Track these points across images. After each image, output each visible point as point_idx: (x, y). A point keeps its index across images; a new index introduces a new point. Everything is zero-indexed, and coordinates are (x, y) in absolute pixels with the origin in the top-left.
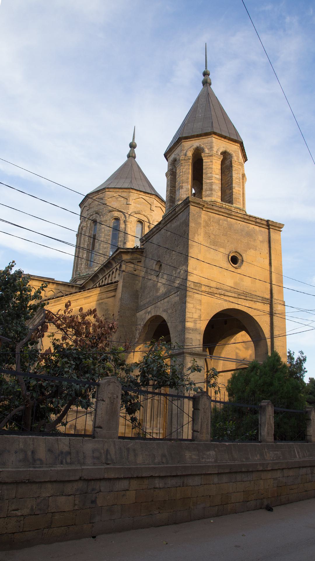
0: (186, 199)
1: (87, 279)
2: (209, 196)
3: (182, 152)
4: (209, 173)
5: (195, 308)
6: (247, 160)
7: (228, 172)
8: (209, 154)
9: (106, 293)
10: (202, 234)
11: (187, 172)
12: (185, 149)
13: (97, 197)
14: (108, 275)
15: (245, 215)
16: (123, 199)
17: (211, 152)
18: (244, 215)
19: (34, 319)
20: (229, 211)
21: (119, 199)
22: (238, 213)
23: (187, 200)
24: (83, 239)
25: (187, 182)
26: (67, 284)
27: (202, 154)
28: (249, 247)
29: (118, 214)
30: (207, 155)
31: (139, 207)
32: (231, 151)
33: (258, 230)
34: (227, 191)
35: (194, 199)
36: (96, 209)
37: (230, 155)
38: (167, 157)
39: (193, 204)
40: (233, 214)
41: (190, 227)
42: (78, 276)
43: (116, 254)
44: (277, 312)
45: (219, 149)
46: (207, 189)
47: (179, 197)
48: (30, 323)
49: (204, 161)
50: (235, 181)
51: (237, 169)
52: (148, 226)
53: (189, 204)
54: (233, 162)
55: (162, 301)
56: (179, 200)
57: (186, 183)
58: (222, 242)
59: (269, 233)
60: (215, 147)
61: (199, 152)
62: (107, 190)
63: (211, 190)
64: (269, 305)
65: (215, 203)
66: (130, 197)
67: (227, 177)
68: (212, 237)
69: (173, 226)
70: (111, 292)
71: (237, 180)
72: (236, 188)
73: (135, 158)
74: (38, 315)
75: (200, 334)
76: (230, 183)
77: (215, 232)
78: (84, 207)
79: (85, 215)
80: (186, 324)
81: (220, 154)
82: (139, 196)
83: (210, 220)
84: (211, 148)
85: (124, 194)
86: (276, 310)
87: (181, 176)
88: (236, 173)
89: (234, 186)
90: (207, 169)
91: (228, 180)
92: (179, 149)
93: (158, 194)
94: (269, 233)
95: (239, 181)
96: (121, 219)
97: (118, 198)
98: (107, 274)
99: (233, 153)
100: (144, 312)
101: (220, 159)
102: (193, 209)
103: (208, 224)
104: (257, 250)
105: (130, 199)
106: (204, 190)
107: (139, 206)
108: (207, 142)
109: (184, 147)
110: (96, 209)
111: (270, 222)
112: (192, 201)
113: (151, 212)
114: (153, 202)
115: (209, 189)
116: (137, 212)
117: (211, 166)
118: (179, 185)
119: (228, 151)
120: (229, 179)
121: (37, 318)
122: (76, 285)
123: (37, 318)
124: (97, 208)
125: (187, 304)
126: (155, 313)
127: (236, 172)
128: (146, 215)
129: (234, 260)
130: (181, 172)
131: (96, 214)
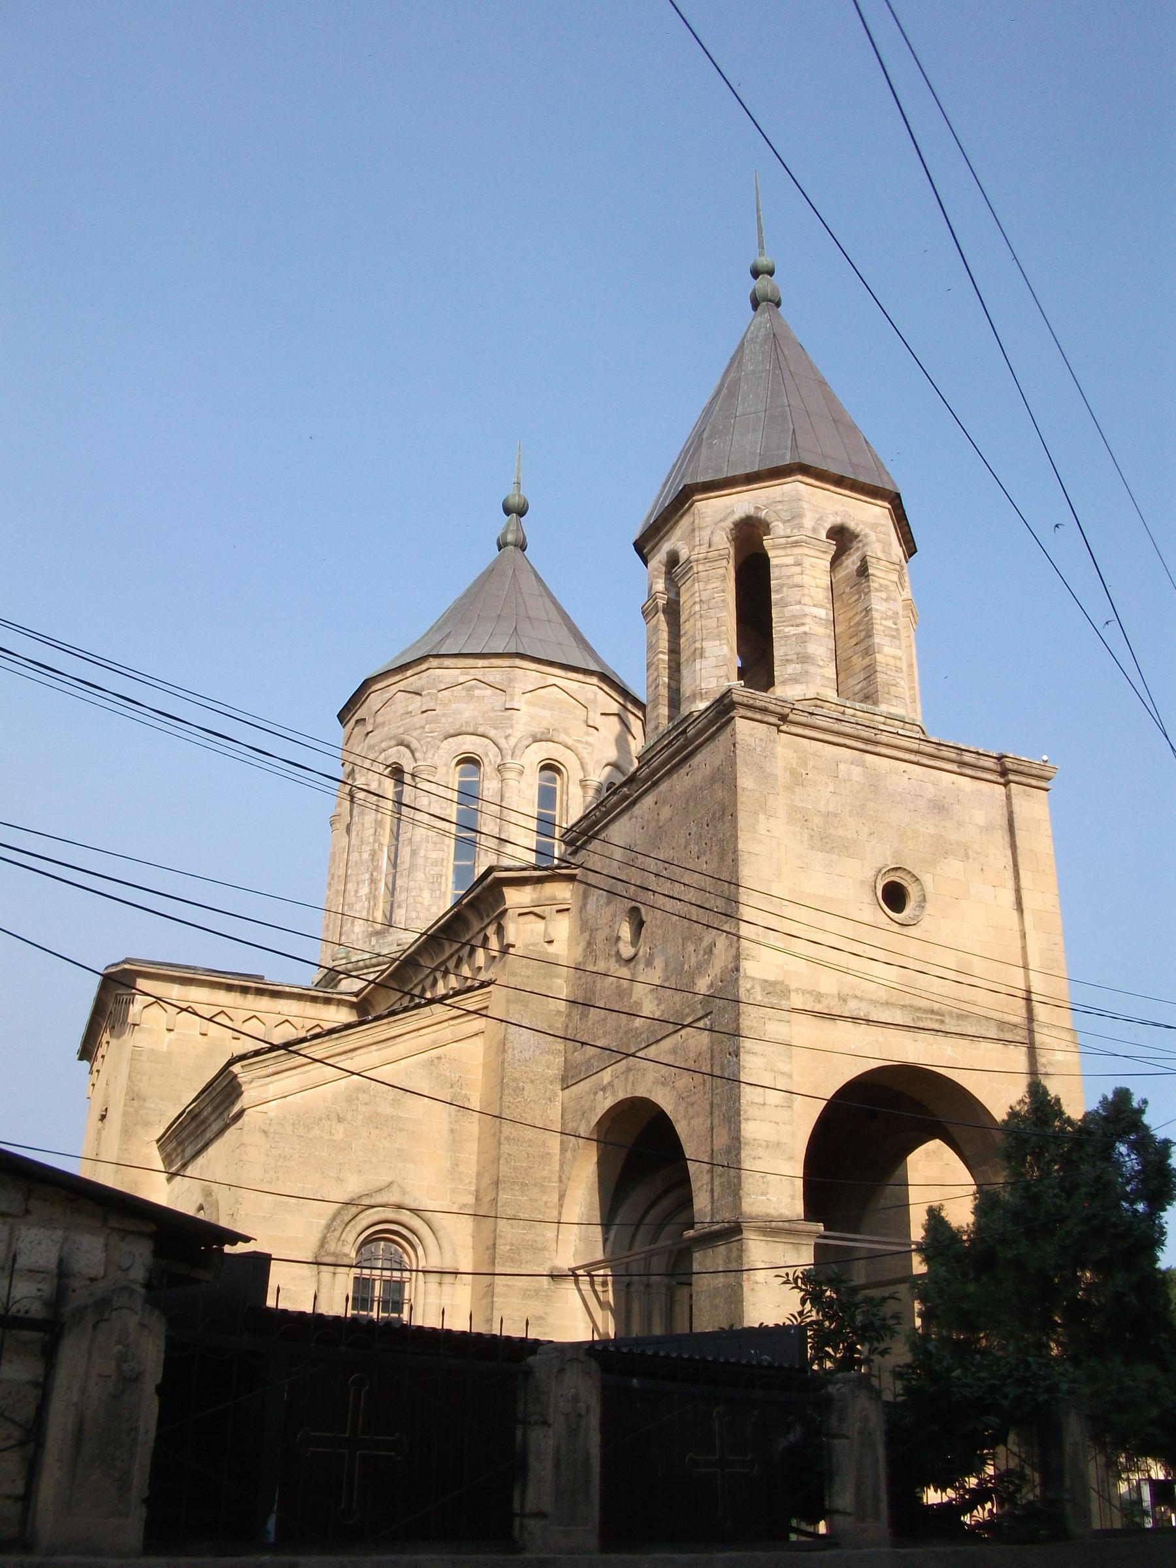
0: (724, 696)
1: (383, 971)
2: (795, 680)
3: (697, 533)
4: (794, 603)
5: (772, 1070)
6: (916, 551)
7: (857, 597)
8: (789, 539)
9: (452, 1022)
10: (782, 813)
11: (714, 600)
12: (705, 525)
13: (401, 686)
14: (455, 958)
15: (922, 743)
16: (489, 691)
17: (795, 530)
18: (917, 741)
19: (203, 1122)
20: (867, 729)
21: (477, 692)
22: (899, 737)
23: (726, 701)
24: (358, 834)
25: (719, 636)
26: (305, 995)
27: (765, 538)
28: (942, 849)
29: (473, 744)
30: (783, 541)
31: (546, 718)
32: (862, 526)
33: (968, 790)
34: (854, 659)
35: (749, 695)
36: (399, 727)
37: (859, 538)
38: (645, 551)
39: (743, 712)
40: (883, 738)
41: (739, 790)
42: (344, 961)
43: (484, 889)
44: (1050, 1070)
45: (821, 519)
46: (788, 657)
47: (693, 687)
48: (188, 1136)
49: (773, 562)
50: (881, 624)
51: (887, 586)
52: (581, 781)
53: (732, 714)
54: (871, 562)
55: (653, 1047)
56: (694, 697)
57: (713, 639)
58: (850, 837)
59: (1009, 797)
60: (807, 513)
61: (755, 531)
62: (434, 662)
63: (804, 659)
64: (1024, 1049)
65: (819, 703)
66: (516, 685)
67: (853, 613)
68: (817, 821)
69: (678, 788)
70: (469, 1021)
71: (889, 623)
72: (886, 650)
73: (524, 550)
74: (217, 1107)
75: (791, 1158)
76: (863, 634)
77: (823, 802)
78: (357, 722)
79: (359, 748)
80: (743, 1126)
81: (825, 537)
82: (545, 679)
83: (804, 762)
84: (795, 518)
85: (493, 676)
86: (1049, 1063)
87: (697, 616)
88: (882, 598)
89: (878, 644)
90: (785, 589)
91: (858, 624)
92: (685, 522)
93: (487, 569)
94: (1009, 797)
95: (895, 624)
96: (486, 761)
97: (471, 688)
98: (451, 956)
99: (867, 531)
100: (587, 1088)
101: (825, 552)
102: (744, 728)
103: (800, 779)
104: (971, 860)
105: (514, 691)
106: (776, 662)
107: (546, 713)
108: (781, 500)
109: (704, 518)
110: (399, 727)
111: (1007, 759)
112: (740, 704)
113: (588, 734)
114: (593, 697)
115: (794, 657)
116: (539, 736)
117: (797, 580)
118: (692, 648)
119: (852, 525)
120: (861, 620)
121: (212, 1118)
122: (339, 997)
123: (212, 1118)
124: (399, 724)
125: (743, 1056)
126: (629, 1089)
127: (883, 595)
128: (570, 742)
129: (895, 896)
130: (695, 603)
131: (398, 745)
